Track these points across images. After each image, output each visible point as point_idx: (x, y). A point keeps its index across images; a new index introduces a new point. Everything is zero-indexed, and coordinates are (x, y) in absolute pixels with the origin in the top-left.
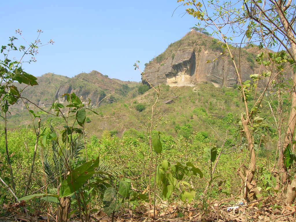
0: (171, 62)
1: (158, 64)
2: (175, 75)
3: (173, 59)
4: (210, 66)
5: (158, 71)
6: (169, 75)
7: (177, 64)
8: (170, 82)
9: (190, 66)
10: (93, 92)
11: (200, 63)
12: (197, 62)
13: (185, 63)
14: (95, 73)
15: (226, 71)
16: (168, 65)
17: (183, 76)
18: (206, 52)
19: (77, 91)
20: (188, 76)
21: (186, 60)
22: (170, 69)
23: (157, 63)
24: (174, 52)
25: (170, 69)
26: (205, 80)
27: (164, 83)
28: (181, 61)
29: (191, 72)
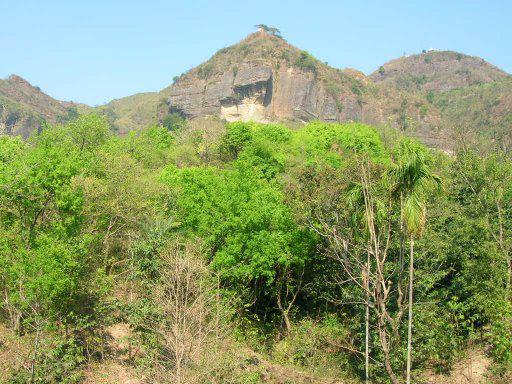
0: (231, 80)
1: (203, 81)
2: (236, 103)
3: (235, 75)
4: (299, 94)
5: (203, 93)
6: (226, 102)
7: (243, 84)
8: (227, 112)
9: (264, 91)
10: (26, 117)
11: (279, 87)
12: (274, 85)
13: (259, 86)
14: (17, 80)
15: (321, 105)
16: (226, 84)
17: (252, 105)
18: (290, 71)
19: (52, 287)
20: (260, 107)
21: (261, 80)
22: (229, 93)
23: (201, 78)
24: (234, 64)
25: (229, 93)
26: (290, 116)
27: (216, 114)
28: (251, 81)
29: (266, 100)
